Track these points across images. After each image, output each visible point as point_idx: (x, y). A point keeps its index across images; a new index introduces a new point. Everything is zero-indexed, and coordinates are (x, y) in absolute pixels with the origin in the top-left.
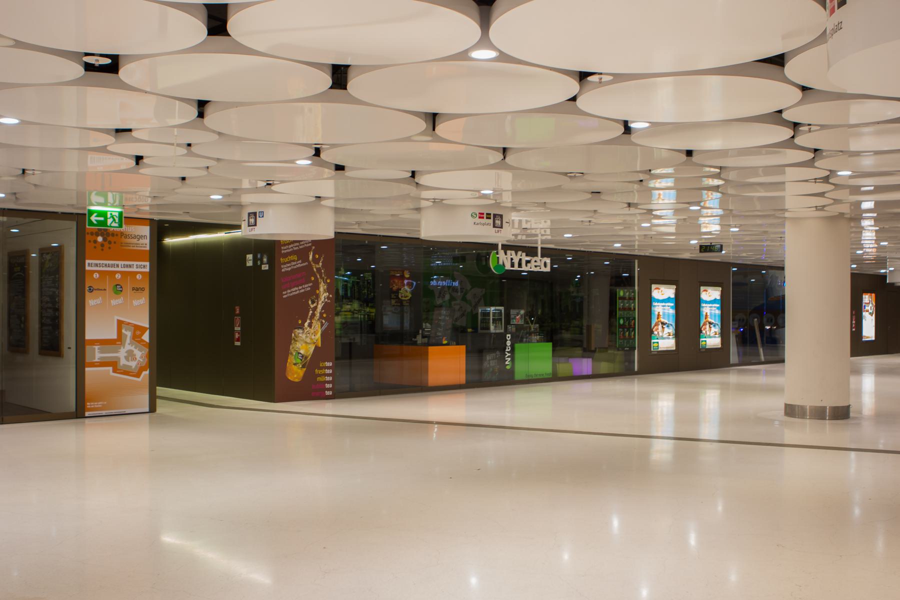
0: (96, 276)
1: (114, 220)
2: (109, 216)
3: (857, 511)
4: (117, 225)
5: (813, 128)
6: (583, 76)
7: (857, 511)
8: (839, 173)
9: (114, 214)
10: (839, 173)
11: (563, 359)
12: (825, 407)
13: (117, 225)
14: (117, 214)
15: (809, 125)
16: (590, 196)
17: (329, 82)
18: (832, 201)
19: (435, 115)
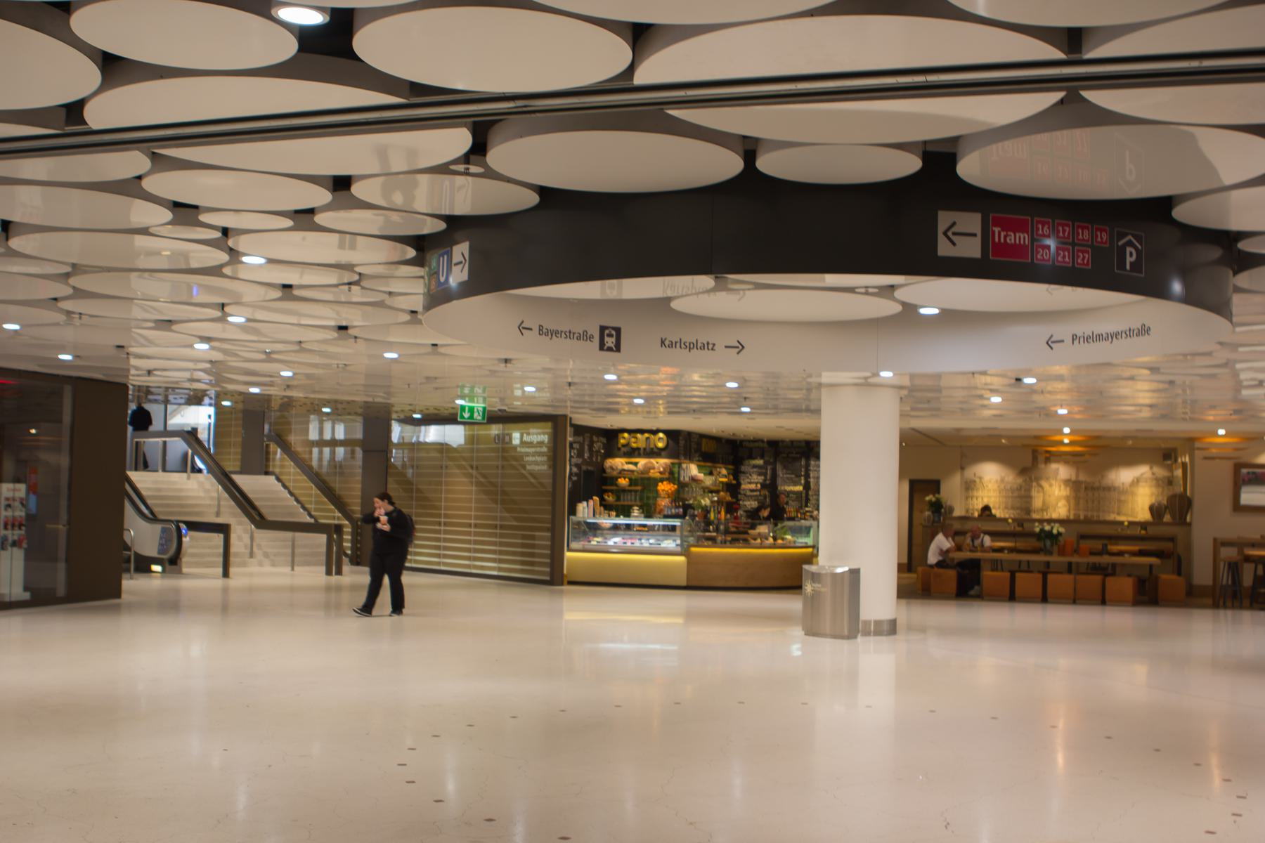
8: (245, 259)
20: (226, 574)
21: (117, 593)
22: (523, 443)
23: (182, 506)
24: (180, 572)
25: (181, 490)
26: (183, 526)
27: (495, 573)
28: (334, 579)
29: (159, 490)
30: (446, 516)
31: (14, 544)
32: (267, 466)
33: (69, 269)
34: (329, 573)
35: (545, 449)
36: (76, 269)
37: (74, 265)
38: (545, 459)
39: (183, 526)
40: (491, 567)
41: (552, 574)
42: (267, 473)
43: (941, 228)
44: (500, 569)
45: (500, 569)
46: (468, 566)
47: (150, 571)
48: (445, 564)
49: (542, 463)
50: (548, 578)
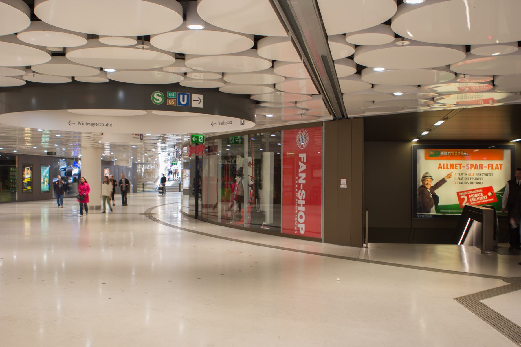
43: (202, 103)
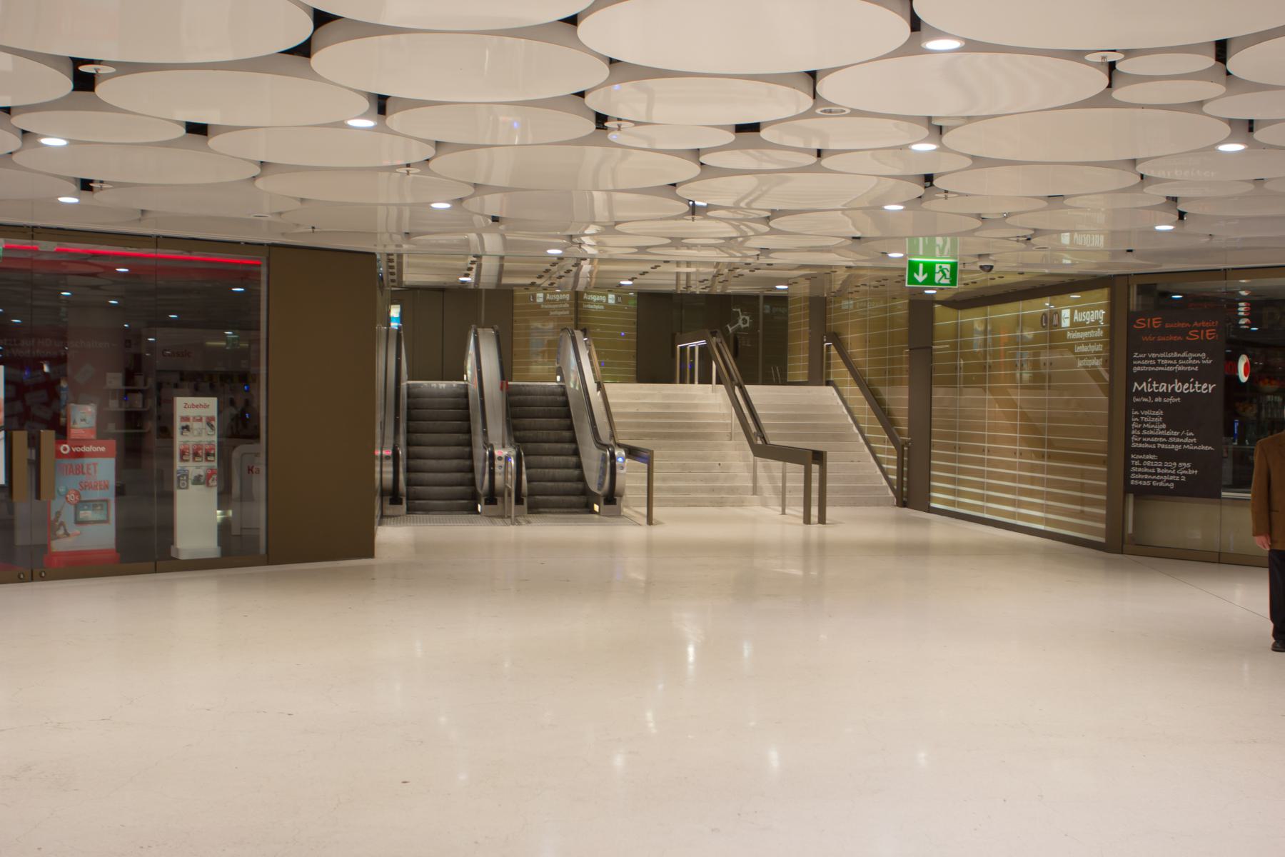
0: (1137, 463)
1: (944, 275)
2: (937, 269)
3: (651, 725)
4: (947, 282)
5: (105, 186)
6: (438, 144)
7: (651, 725)
8: (44, 141)
9: (944, 266)
10: (44, 141)
11: (697, 289)
12: (700, 382)
13: (947, 282)
14: (948, 267)
15: (619, 120)
16: (1044, 204)
17: (593, 126)
18: (969, 162)
19: (1251, 122)
20: (650, 521)
21: (365, 548)
22: (1074, 325)
23: (690, 426)
24: (618, 514)
25: (696, 406)
26: (619, 453)
27: (1042, 527)
28: (815, 530)
29: (668, 406)
30: (991, 428)
31: (197, 481)
32: (828, 374)
33: (768, 214)
34: (807, 520)
35: (1100, 333)
36: (775, 214)
37: (773, 211)
38: (1099, 348)
39: (619, 453)
40: (1034, 515)
41: (1109, 532)
42: (828, 383)
44: (1047, 522)
45: (1047, 522)
46: (1012, 515)
47: (1219, 496)
48: (990, 510)
49: (1097, 355)
50: (1102, 540)
